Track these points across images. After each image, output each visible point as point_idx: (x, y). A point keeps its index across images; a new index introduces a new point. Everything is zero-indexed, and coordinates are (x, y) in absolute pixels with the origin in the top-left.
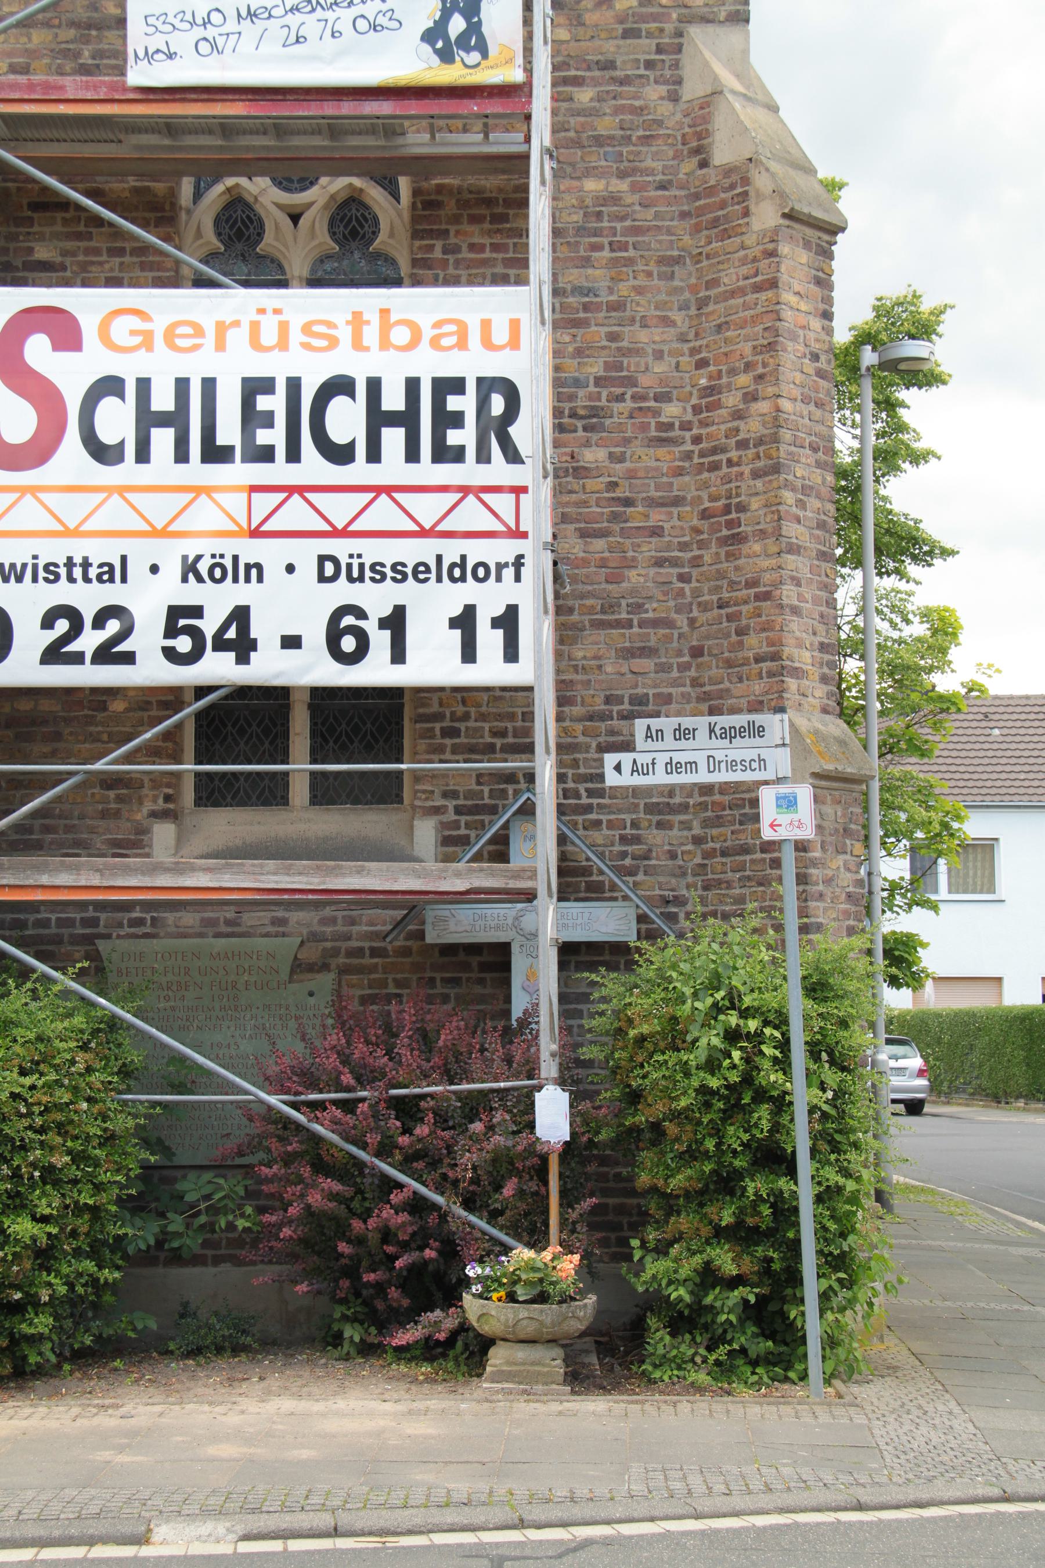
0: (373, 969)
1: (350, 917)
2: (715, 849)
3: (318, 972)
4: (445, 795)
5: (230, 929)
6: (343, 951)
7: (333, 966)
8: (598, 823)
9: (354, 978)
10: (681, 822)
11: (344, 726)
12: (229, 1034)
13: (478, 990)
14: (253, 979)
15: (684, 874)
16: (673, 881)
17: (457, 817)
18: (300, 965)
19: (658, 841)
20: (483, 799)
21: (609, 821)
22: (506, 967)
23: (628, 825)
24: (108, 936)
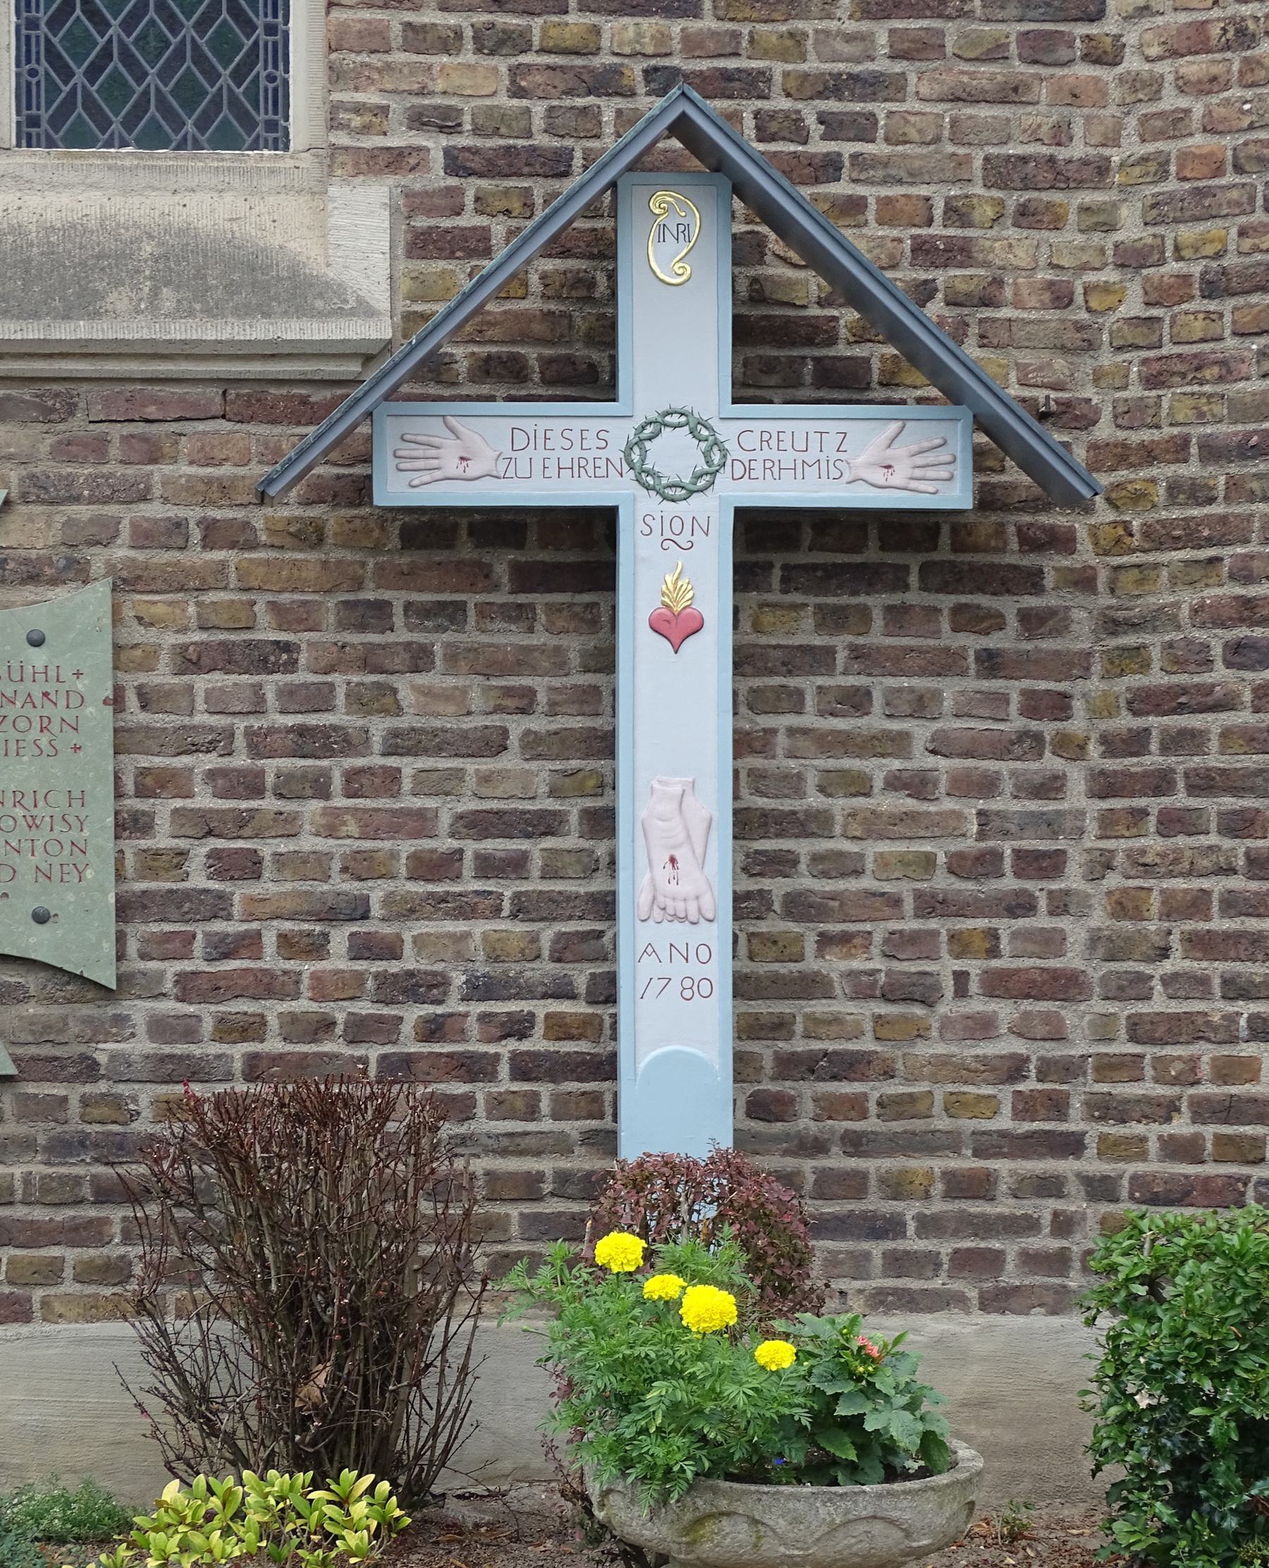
1: (144, 439)
2: (1186, 279)
3: (54, 582)
4: (418, 120)
6: (125, 527)
7: (97, 567)
8: (854, 206)
9: (158, 604)
10: (1085, 210)
11: (79, 77)
13: (509, 637)
15: (1091, 346)
16: (1060, 363)
17: (453, 181)
19: (1021, 256)
20: (529, 135)
21: (886, 202)
22: (602, 575)
23: (938, 212)
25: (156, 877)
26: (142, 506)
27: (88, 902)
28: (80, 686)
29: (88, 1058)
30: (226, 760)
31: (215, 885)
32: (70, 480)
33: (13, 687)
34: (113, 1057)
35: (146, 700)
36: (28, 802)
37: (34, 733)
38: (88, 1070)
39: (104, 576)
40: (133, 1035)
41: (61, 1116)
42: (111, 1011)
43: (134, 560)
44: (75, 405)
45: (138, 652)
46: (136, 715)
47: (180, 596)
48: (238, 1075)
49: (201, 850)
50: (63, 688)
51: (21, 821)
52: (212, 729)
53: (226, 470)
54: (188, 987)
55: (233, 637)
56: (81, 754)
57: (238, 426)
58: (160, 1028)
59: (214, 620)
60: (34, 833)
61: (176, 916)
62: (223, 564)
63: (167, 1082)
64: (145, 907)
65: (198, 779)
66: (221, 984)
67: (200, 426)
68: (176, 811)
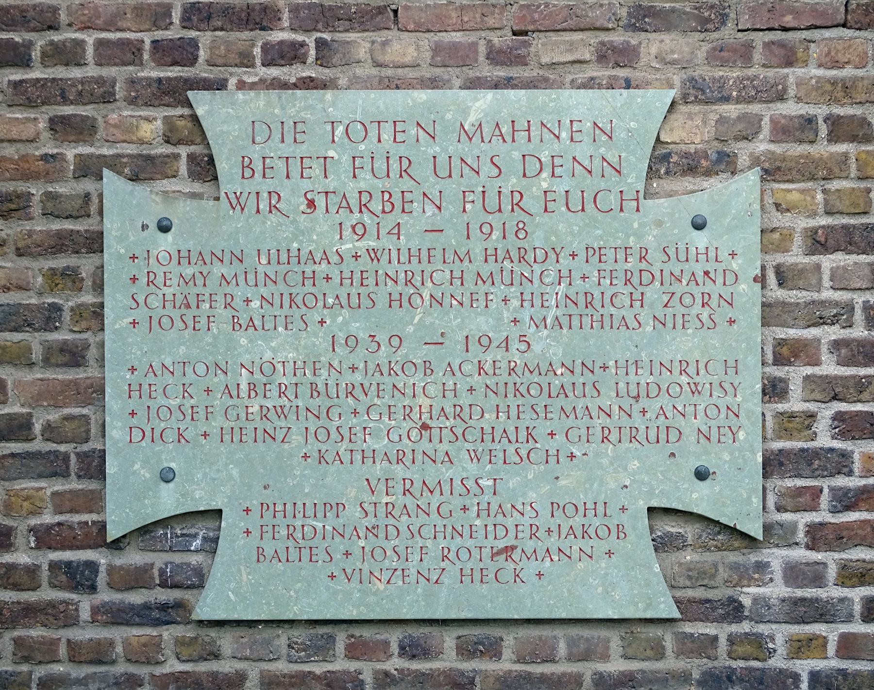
0: (833, 169)
1: (782, 45)
3: (708, 173)
5: (501, 72)
6: (766, 123)
7: (743, 160)
12: (507, 316)
14: (560, 187)
18: (666, 157)
24: (220, 85)
25: (791, 437)
26: (779, 105)
27: (740, 461)
28: (735, 266)
29: (735, 601)
30: (848, 330)
31: (837, 444)
32: (721, 83)
33: (680, 266)
34: (756, 600)
35: (783, 277)
36: (691, 370)
37: (697, 308)
38: (734, 611)
39: (750, 168)
40: (771, 580)
41: (711, 652)
42: (753, 558)
43: (773, 153)
44: (727, 15)
45: (776, 236)
46: (778, 294)
47: (810, 185)
48: (857, 616)
49: (827, 412)
50: (721, 267)
51: (686, 388)
52: (837, 304)
53: (848, 72)
54: (817, 537)
55: (852, 221)
56: (735, 326)
57: (858, 33)
58: (794, 574)
59: (839, 206)
60: (696, 399)
61: (808, 472)
62: (846, 155)
63: (799, 623)
64: (781, 464)
65: (824, 349)
66: (845, 533)
67: (827, 33)
68: (807, 378)
